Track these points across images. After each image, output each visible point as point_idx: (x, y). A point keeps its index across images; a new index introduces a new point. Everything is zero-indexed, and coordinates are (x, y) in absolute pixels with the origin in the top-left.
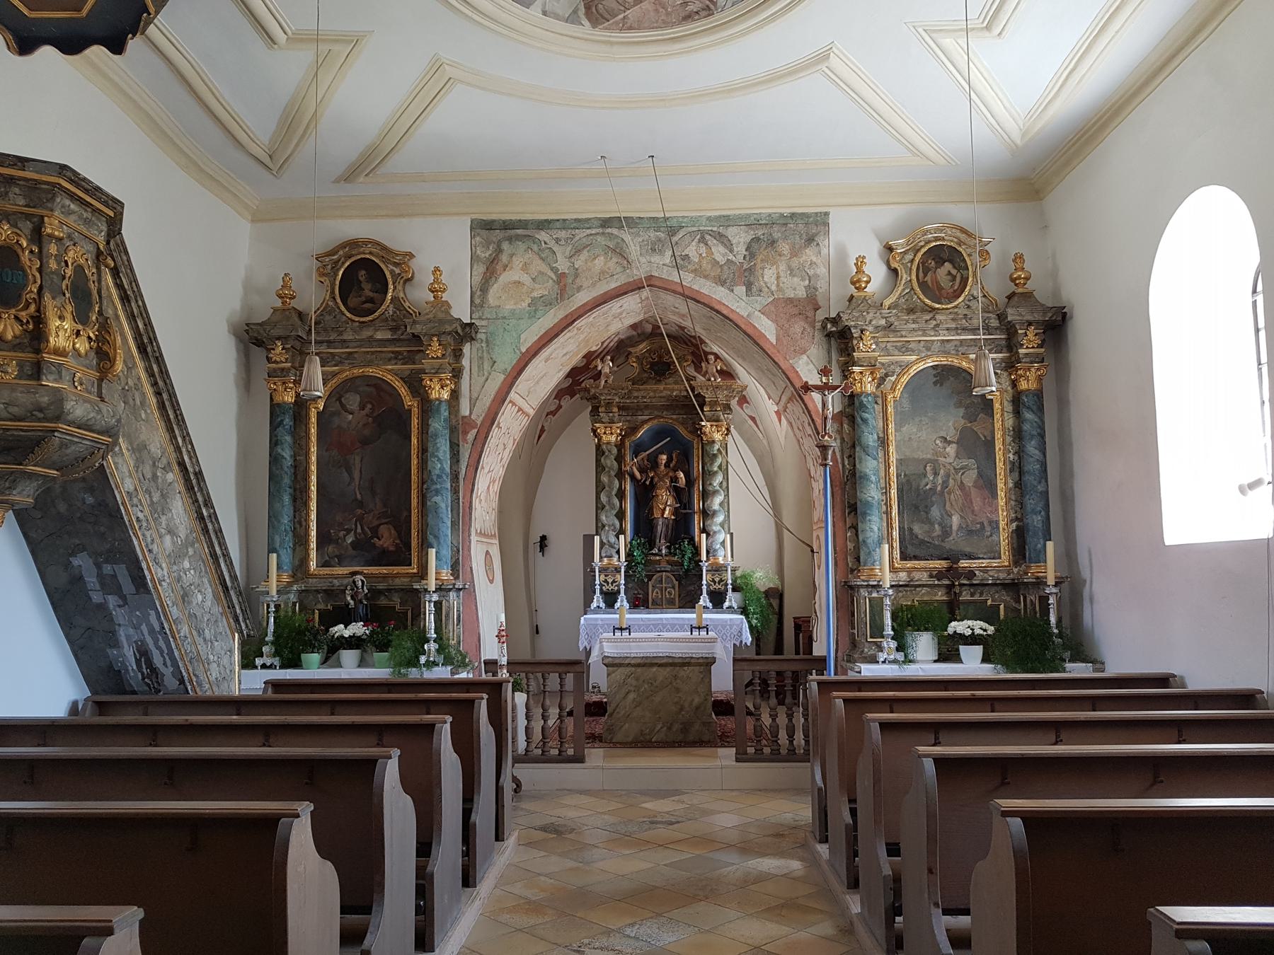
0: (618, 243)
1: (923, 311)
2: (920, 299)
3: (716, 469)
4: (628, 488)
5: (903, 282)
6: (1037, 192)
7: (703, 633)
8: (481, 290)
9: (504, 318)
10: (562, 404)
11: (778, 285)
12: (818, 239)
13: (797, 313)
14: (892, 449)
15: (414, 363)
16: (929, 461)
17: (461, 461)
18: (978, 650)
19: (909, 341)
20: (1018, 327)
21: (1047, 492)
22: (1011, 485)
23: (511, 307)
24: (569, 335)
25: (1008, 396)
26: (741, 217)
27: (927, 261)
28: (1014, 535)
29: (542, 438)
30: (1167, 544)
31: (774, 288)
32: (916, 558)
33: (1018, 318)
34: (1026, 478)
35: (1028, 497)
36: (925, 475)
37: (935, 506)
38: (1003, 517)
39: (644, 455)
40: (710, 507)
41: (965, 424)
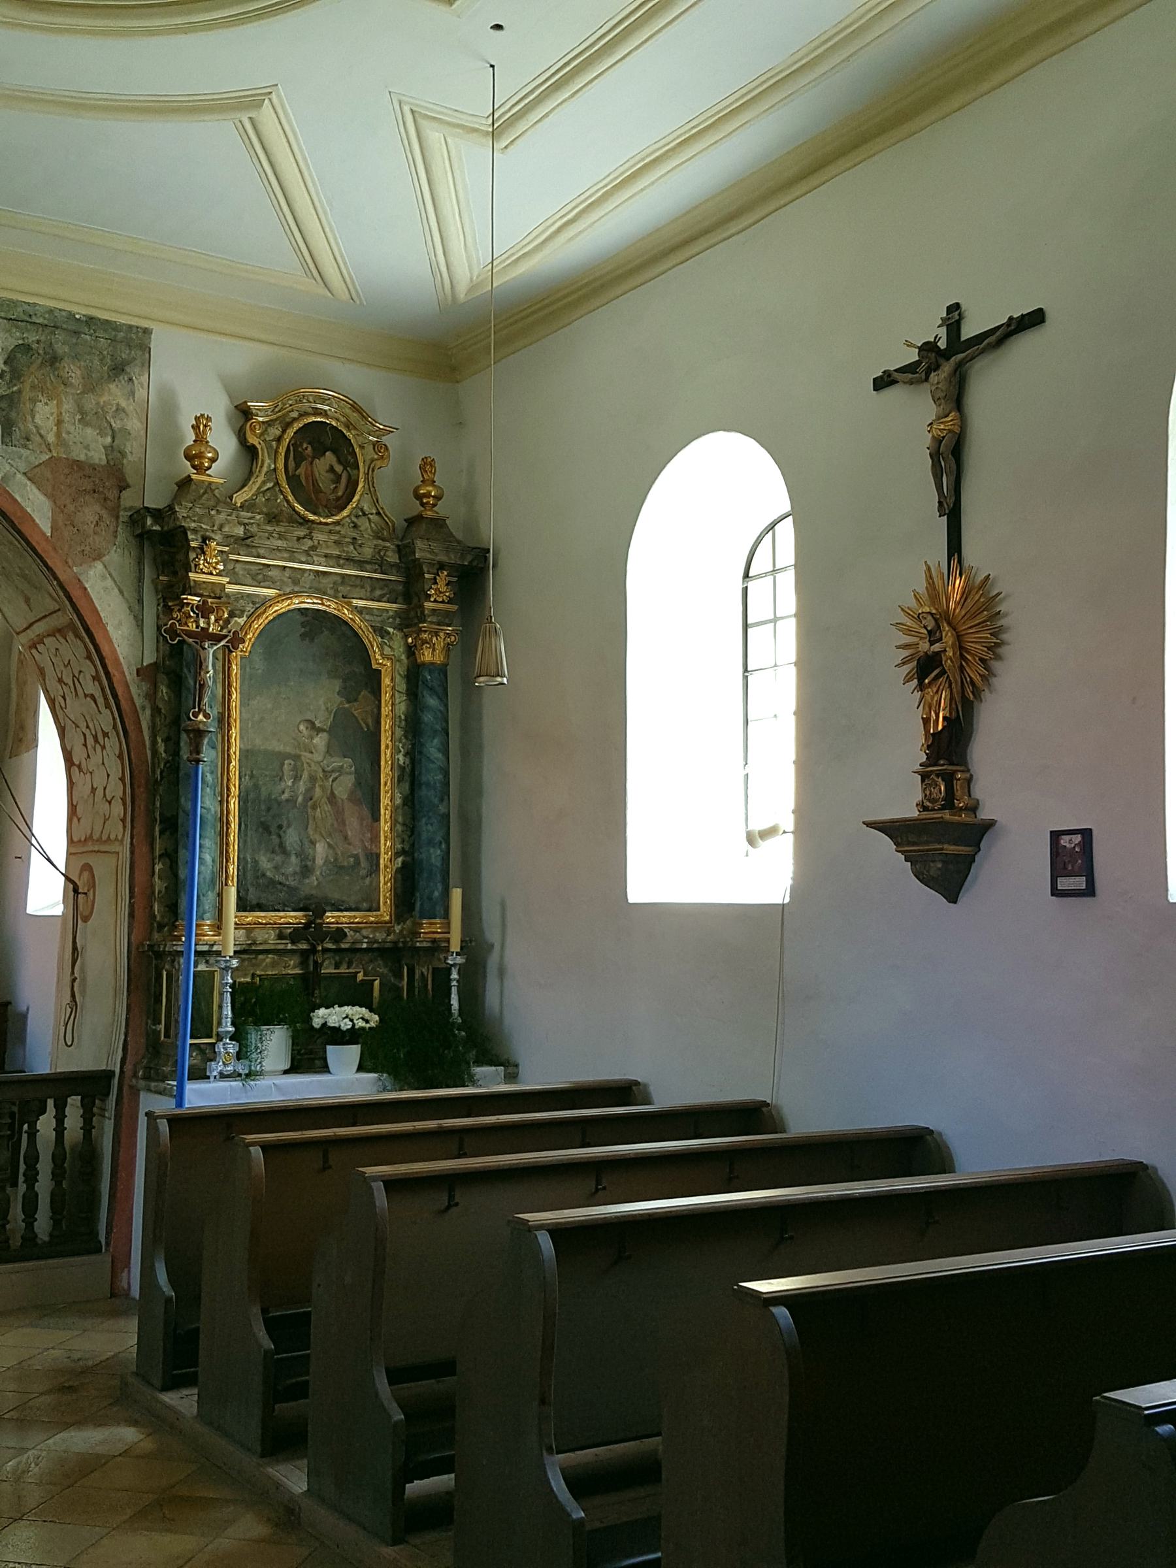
1: (291, 521)
2: (288, 501)
5: (265, 469)
6: (454, 369)
11: (58, 435)
12: (134, 370)
13: (90, 487)
14: (234, 732)
16: (288, 756)
18: (353, 1052)
19: (269, 566)
20: (425, 570)
21: (449, 815)
22: (398, 801)
25: (402, 669)
27: (301, 445)
28: (399, 876)
30: (630, 901)
31: (51, 438)
32: (260, 907)
33: (429, 556)
34: (424, 792)
35: (424, 820)
38: (385, 848)
41: (341, 703)
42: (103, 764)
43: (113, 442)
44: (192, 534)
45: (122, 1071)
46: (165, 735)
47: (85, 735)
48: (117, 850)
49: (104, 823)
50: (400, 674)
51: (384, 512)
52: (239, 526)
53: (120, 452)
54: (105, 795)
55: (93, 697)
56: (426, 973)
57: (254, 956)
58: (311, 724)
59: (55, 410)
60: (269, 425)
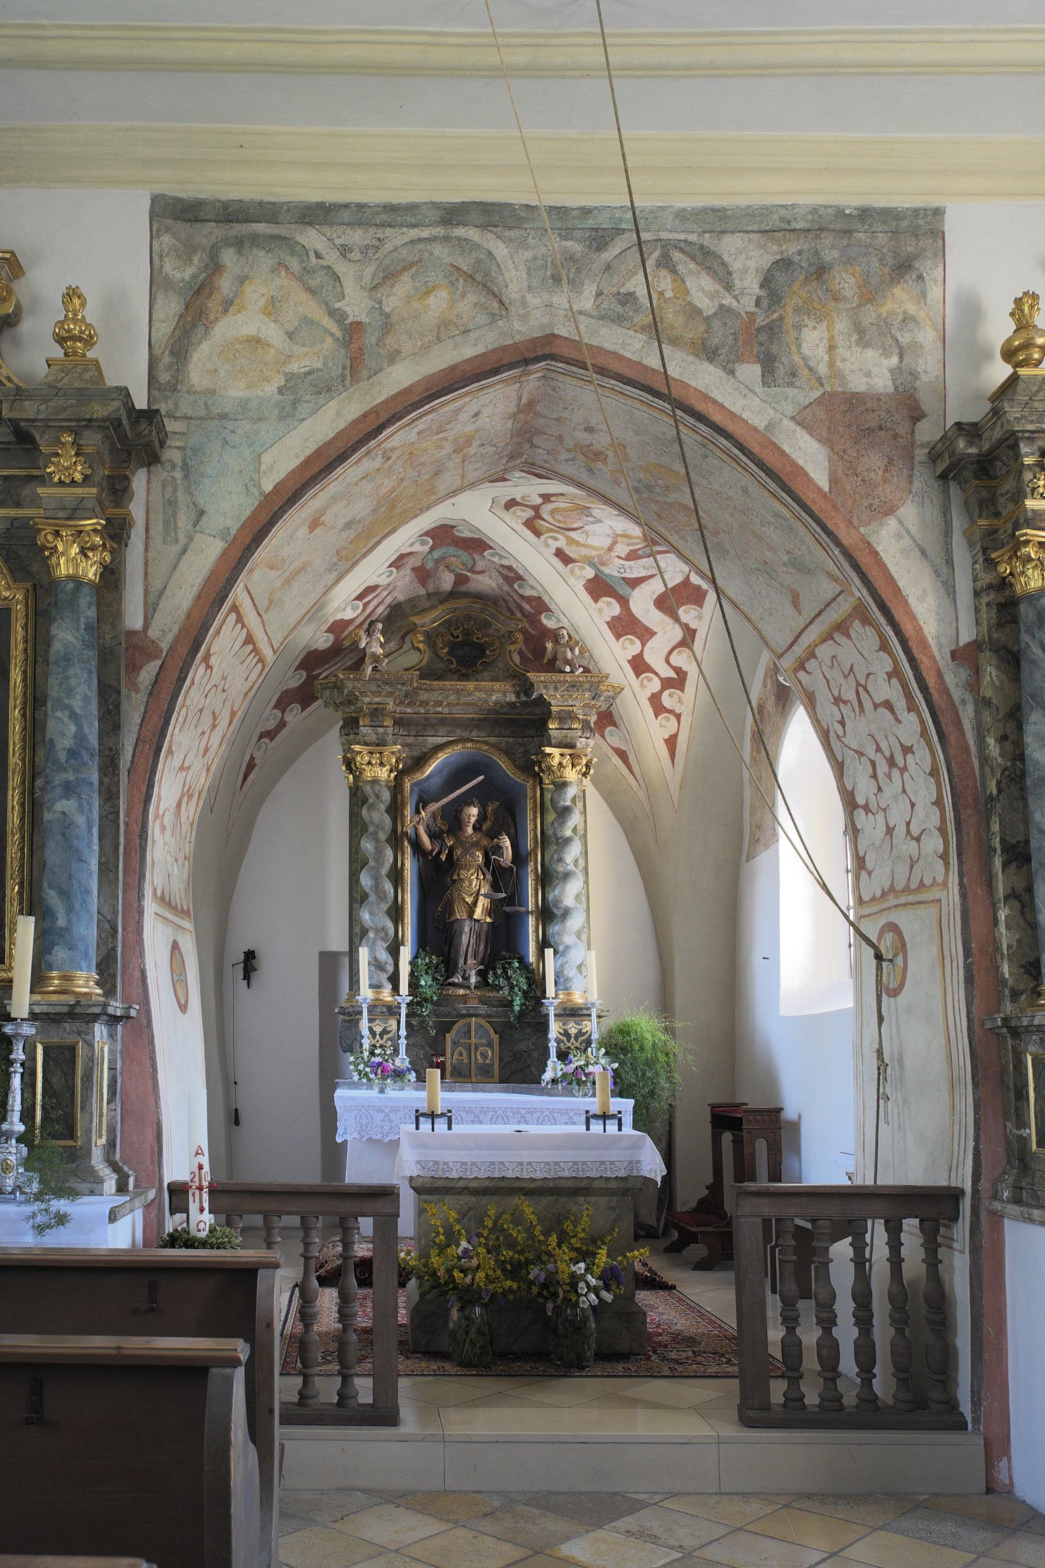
0: (479, 262)
3: (568, 833)
4: (408, 864)
7: (612, 1127)
8: (172, 353)
9: (224, 417)
10: (286, 719)
11: (831, 364)
12: (924, 266)
15: (18, 505)
17: (124, 730)
23: (241, 394)
24: (368, 465)
26: (750, 214)
29: (251, 777)
39: (434, 807)
40: (557, 902)
42: (904, 791)
43: (901, 362)
44: (1026, 445)
45: (975, 1191)
46: (1000, 733)
47: (873, 764)
48: (937, 897)
49: (912, 867)
53: (910, 374)
54: (908, 832)
55: (888, 705)
59: (825, 334)
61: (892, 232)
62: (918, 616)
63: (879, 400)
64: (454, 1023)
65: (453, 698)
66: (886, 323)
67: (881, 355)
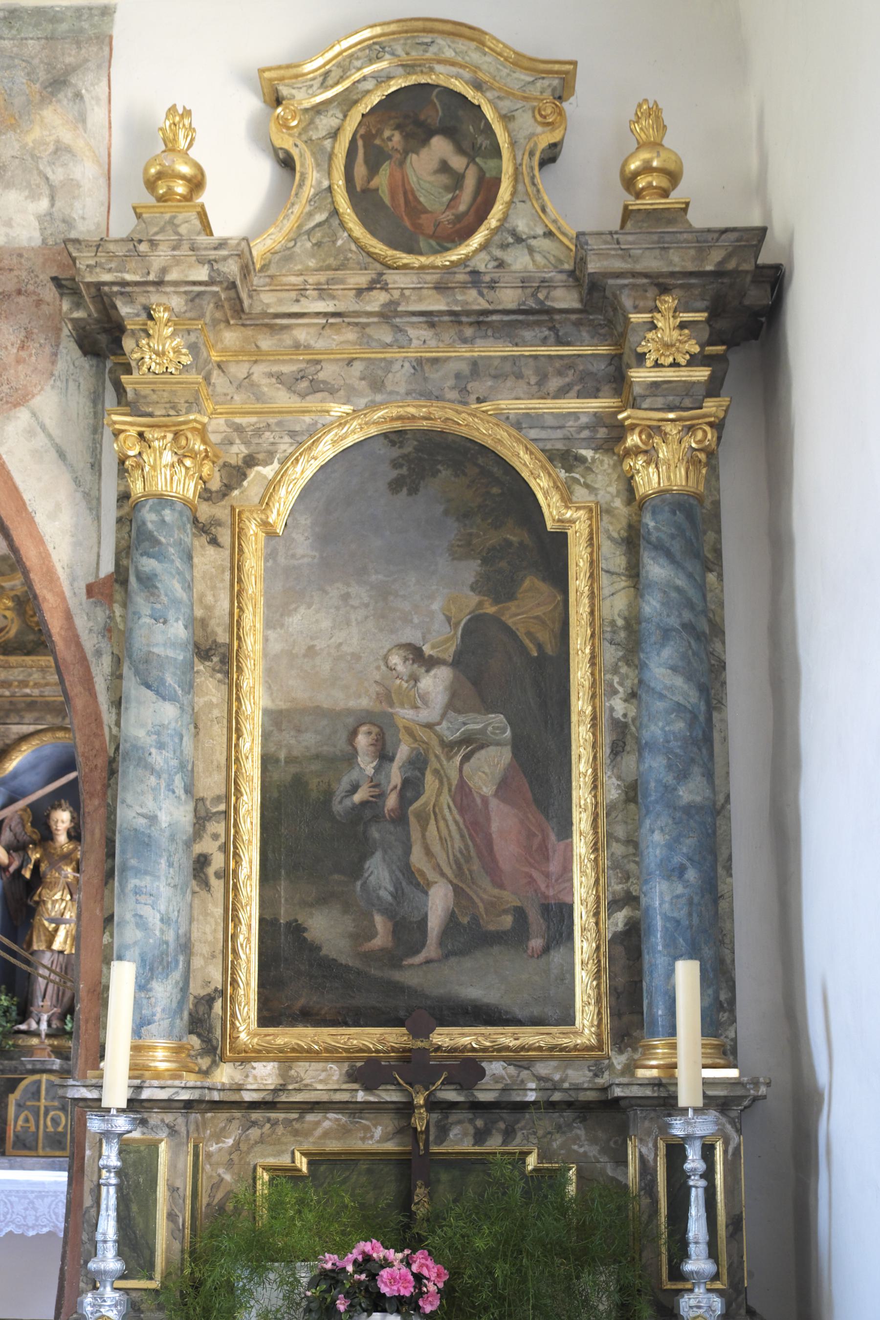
2: (355, 241)
16: (366, 718)
20: (627, 301)
27: (380, 132)
36: (350, 758)
37: (378, 855)
41: (480, 604)
44: (125, 304)
50: (610, 538)
51: (559, 229)
52: (200, 266)
53: (64, 221)
56: (651, 1158)
57: (296, 1116)
58: (415, 653)
60: (319, 112)
61: (46, 38)
62: (47, 538)
63: (20, 256)
64: (24, 1079)
65: (36, 676)
66: (33, 156)
67: (26, 198)
